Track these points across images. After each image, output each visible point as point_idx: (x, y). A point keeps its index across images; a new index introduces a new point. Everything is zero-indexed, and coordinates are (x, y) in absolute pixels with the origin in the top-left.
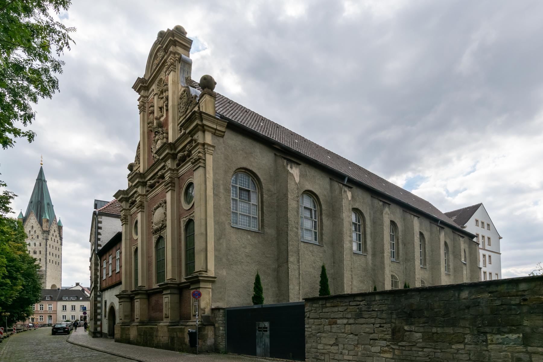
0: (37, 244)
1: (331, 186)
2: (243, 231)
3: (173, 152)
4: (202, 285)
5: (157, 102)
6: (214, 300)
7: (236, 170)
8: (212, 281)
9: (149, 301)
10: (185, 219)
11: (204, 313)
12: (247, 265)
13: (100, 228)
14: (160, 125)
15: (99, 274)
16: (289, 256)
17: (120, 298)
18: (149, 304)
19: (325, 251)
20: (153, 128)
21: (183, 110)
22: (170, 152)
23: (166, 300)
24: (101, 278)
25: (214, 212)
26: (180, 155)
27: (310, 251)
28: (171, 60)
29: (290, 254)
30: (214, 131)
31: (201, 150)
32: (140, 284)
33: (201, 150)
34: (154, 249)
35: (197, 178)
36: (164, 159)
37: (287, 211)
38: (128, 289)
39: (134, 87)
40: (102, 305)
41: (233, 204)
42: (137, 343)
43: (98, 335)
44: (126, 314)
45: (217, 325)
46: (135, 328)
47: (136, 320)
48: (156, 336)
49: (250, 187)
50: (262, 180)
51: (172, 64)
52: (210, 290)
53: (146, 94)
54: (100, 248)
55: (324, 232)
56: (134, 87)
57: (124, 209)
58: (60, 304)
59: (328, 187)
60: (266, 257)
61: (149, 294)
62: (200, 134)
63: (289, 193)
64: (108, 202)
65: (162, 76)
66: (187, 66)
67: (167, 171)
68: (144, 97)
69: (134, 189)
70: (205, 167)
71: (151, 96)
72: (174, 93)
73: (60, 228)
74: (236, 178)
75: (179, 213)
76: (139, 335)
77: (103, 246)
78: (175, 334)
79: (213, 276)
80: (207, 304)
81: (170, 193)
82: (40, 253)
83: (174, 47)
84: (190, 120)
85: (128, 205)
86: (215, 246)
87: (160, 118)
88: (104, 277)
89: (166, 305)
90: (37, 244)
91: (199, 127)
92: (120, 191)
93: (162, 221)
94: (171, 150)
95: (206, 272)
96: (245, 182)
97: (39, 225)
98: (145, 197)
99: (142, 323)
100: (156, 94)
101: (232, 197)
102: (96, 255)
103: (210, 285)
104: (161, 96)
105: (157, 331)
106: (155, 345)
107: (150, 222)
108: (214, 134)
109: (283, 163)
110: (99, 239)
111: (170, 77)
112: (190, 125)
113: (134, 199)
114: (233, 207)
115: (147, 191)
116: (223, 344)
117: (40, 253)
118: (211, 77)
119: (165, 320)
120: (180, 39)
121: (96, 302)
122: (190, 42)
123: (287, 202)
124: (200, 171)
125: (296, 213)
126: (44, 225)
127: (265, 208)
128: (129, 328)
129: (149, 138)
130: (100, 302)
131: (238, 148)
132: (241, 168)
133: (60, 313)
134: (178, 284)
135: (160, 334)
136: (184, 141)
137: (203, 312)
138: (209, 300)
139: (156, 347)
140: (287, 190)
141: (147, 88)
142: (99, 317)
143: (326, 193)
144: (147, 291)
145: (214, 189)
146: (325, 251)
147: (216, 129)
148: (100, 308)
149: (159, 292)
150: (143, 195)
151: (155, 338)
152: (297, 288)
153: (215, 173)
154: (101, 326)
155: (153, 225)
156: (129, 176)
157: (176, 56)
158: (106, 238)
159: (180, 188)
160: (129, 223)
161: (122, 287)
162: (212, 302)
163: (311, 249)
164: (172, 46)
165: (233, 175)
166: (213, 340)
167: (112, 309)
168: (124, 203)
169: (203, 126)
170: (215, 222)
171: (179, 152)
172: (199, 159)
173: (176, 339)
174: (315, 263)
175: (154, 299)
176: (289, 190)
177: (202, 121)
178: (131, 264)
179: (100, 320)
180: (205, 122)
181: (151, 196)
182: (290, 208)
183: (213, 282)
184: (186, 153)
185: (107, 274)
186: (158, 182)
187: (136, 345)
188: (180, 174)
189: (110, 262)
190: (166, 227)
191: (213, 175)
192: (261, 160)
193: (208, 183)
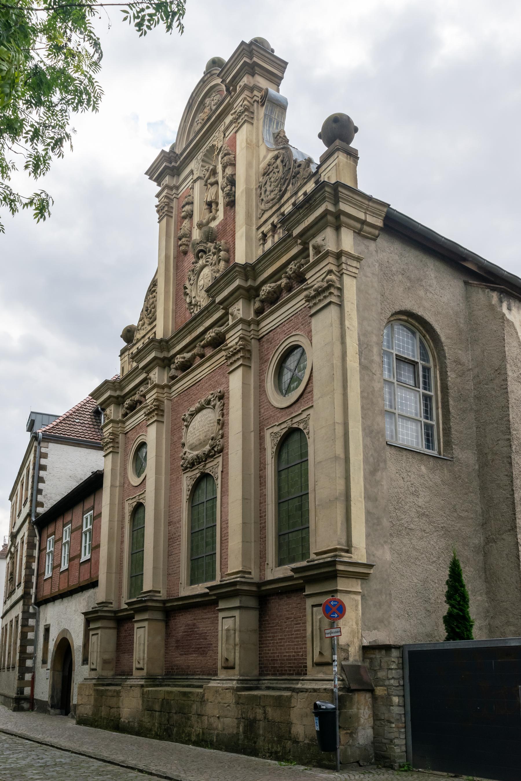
3: (250, 283)
4: (342, 584)
5: (201, 193)
6: (368, 625)
8: (362, 573)
11: (346, 659)
12: (421, 538)
13: (43, 468)
14: (210, 236)
15: (35, 566)
18: (168, 635)
22: (243, 284)
23: (229, 626)
24: (40, 574)
25: (362, 407)
28: (246, 102)
30: (358, 226)
31: (334, 268)
33: (334, 268)
34: (185, 505)
37: (506, 407)
38: (112, 599)
40: (36, 636)
42: (140, 731)
43: (26, 705)
44: (107, 657)
45: (380, 691)
46: (137, 692)
47: (136, 673)
48: (200, 715)
49: (416, 357)
50: (443, 339)
51: (246, 110)
52: (359, 598)
53: (174, 182)
54: (41, 510)
56: (150, 173)
57: (112, 421)
60: (460, 518)
62: (329, 233)
63: (508, 366)
64: (57, 417)
66: (277, 111)
67: (234, 326)
68: (171, 188)
69: (141, 373)
70: (341, 306)
72: (249, 165)
75: (260, 416)
76: (149, 709)
78: (260, 711)
79: (364, 560)
80: (353, 633)
81: (240, 371)
83: (250, 77)
85: (121, 411)
87: (208, 223)
88: (48, 574)
89: (228, 637)
92: (106, 382)
93: (212, 439)
94: (246, 280)
95: (348, 551)
96: (406, 344)
99: (152, 680)
100: (199, 178)
102: (32, 524)
103: (356, 586)
104: (212, 180)
105: (203, 701)
106: (194, 738)
107: (175, 442)
108: (358, 233)
109: (489, 299)
110: (40, 492)
111: (242, 138)
112: (306, 216)
113: (137, 397)
115: (173, 378)
116: (400, 743)
118: (349, 118)
119: (222, 674)
120: (265, 62)
121: (26, 629)
122: (283, 65)
123: (504, 389)
124: (332, 312)
127: (451, 402)
128: (118, 693)
129: (177, 267)
131: (394, 270)
132: (401, 312)
134: (259, 585)
135: (211, 709)
136: (279, 258)
137: (343, 655)
138: (357, 624)
139: (196, 744)
140: (504, 358)
141: (176, 172)
142: (29, 663)
144: (164, 602)
145: (360, 353)
147: (364, 222)
148: (33, 642)
149: (208, 603)
150: (163, 387)
151: (194, 718)
153: (361, 319)
157: (256, 93)
158: (57, 486)
160: (120, 450)
161: (99, 594)
162: (363, 630)
165: (385, 327)
166: (370, 732)
167: (64, 647)
169: (338, 214)
170: (364, 429)
171: (264, 282)
173: (262, 724)
175: (182, 622)
176: (508, 358)
177: (336, 203)
178: (122, 542)
179: (32, 670)
180: (344, 207)
181: (179, 387)
183: (364, 577)
185: (56, 567)
186: (202, 356)
187: (138, 734)
189: (66, 539)
191: (359, 323)
192: (440, 296)
193: (348, 340)
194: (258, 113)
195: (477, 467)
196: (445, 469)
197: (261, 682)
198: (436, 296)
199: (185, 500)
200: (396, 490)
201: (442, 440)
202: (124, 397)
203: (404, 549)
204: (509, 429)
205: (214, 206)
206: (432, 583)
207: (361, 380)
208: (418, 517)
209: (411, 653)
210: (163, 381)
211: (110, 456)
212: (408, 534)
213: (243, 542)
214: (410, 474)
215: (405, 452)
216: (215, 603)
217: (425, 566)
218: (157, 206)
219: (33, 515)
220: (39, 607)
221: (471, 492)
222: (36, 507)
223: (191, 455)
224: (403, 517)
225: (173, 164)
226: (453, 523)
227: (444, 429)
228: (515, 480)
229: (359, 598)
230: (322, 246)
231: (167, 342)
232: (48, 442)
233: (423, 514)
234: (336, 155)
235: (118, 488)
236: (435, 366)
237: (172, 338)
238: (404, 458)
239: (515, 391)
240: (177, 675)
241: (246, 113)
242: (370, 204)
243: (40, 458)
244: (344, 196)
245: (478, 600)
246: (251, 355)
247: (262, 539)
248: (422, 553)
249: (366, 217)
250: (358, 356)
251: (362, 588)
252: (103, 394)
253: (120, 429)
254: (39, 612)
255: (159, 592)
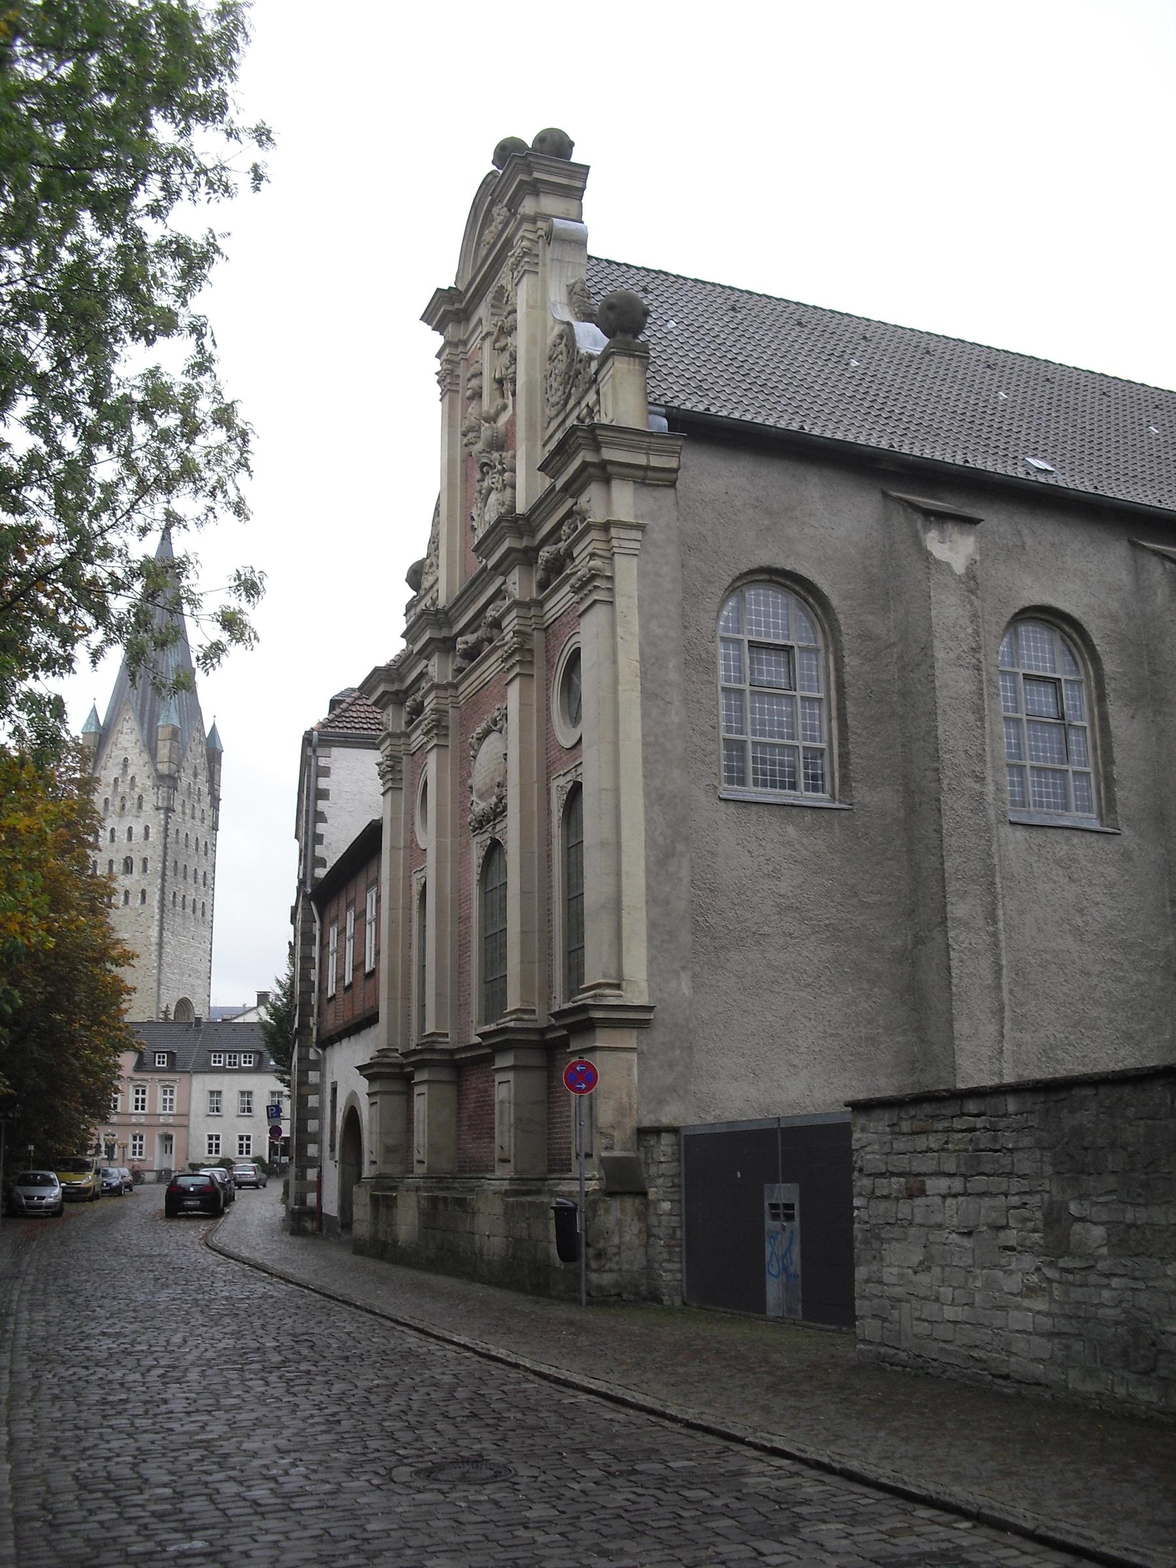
0: (138, 830)
1: (1137, 571)
2: (764, 812)
5: (492, 359)
7: (734, 581)
8: (637, 1020)
9: (460, 1093)
10: (562, 781)
12: (784, 948)
13: (323, 794)
16: (951, 898)
17: (371, 1078)
19: (1126, 856)
20: (476, 453)
21: (554, 399)
24: (323, 990)
25: (645, 760)
26: (544, 554)
27: (1058, 862)
29: (953, 887)
30: (640, 473)
32: (430, 1028)
34: (475, 891)
35: (589, 636)
36: (502, 568)
37: (932, 714)
39: (426, 317)
41: (728, 708)
43: (309, 1225)
44: (390, 1141)
50: (835, 602)
54: (321, 873)
55: (1116, 771)
56: (426, 317)
57: (389, 735)
58: (201, 1084)
59: (1124, 577)
61: (463, 1067)
63: (936, 643)
65: (504, 278)
67: (509, 610)
71: (475, 341)
72: (532, 341)
73: (214, 756)
74: (739, 610)
77: (330, 864)
79: (643, 1001)
80: (622, 1111)
81: (516, 684)
82: (145, 870)
84: (563, 452)
85: (405, 717)
86: (648, 887)
90: (138, 830)
91: (591, 470)
95: (618, 986)
97: (146, 757)
98: (450, 692)
100: (488, 334)
101: (722, 683)
103: (629, 1039)
112: (565, 465)
114: (728, 719)
117: (145, 870)
121: (305, 1090)
122: (583, 171)
123: (931, 678)
124: (598, 615)
125: (971, 718)
126: (164, 751)
127: (851, 708)
130: (317, 1089)
132: (751, 572)
133: (201, 1128)
138: (629, 1096)
140: (929, 631)
142: (312, 1150)
143: (1116, 604)
144: (452, 1052)
145: (644, 674)
146: (1126, 856)
148: (317, 1113)
150: (444, 687)
152: (992, 1029)
153: (646, 618)
154: (318, 1186)
155: (474, 798)
156: (410, 607)
159: (550, 664)
160: (404, 784)
163: (1062, 850)
164: (533, 178)
167: (352, 1117)
168: (390, 710)
170: (647, 795)
172: (593, 577)
174: (1081, 911)
175: (474, 1081)
179: (316, 1162)
180: (608, 454)
182: (943, 698)
184: (562, 545)
185: (340, 978)
186: (490, 641)
188: (550, 616)
190: (505, 808)
191: (641, 627)
192: (831, 528)
194: (544, 255)
195: (902, 814)
196: (836, 826)
197: (547, 1183)
198: (822, 531)
199: (475, 882)
200: (736, 873)
201: (837, 775)
202: (407, 692)
203: (749, 969)
204: (937, 751)
205: (508, 386)
206: (803, 1020)
207: (643, 716)
208: (779, 913)
209: (691, 1139)
210: (446, 677)
211: (389, 794)
212: (758, 943)
213: (522, 962)
214: (763, 843)
215: (754, 808)
216: (488, 1059)
217: (791, 993)
218: (437, 374)
219: (309, 882)
220: (324, 1049)
221: (889, 859)
222: (313, 869)
223: (480, 807)
224: (749, 916)
225: (457, 306)
226: (850, 916)
227: (840, 755)
228: (946, 839)
229: (634, 1056)
230: (587, 511)
231: (446, 613)
232: (330, 746)
233: (790, 908)
234: (610, 363)
235: (402, 852)
236: (827, 647)
237: (451, 608)
238: (754, 817)
239: (951, 683)
240: (470, 1171)
241: (526, 259)
242: (653, 440)
243: (317, 777)
244: (607, 439)
245: (898, 1042)
246: (613, 597)
247: (547, 956)
248: (785, 973)
249: (648, 460)
250: (638, 680)
251: (639, 1042)
252: (375, 688)
253: (402, 747)
254: (325, 1059)
255: (446, 1035)
